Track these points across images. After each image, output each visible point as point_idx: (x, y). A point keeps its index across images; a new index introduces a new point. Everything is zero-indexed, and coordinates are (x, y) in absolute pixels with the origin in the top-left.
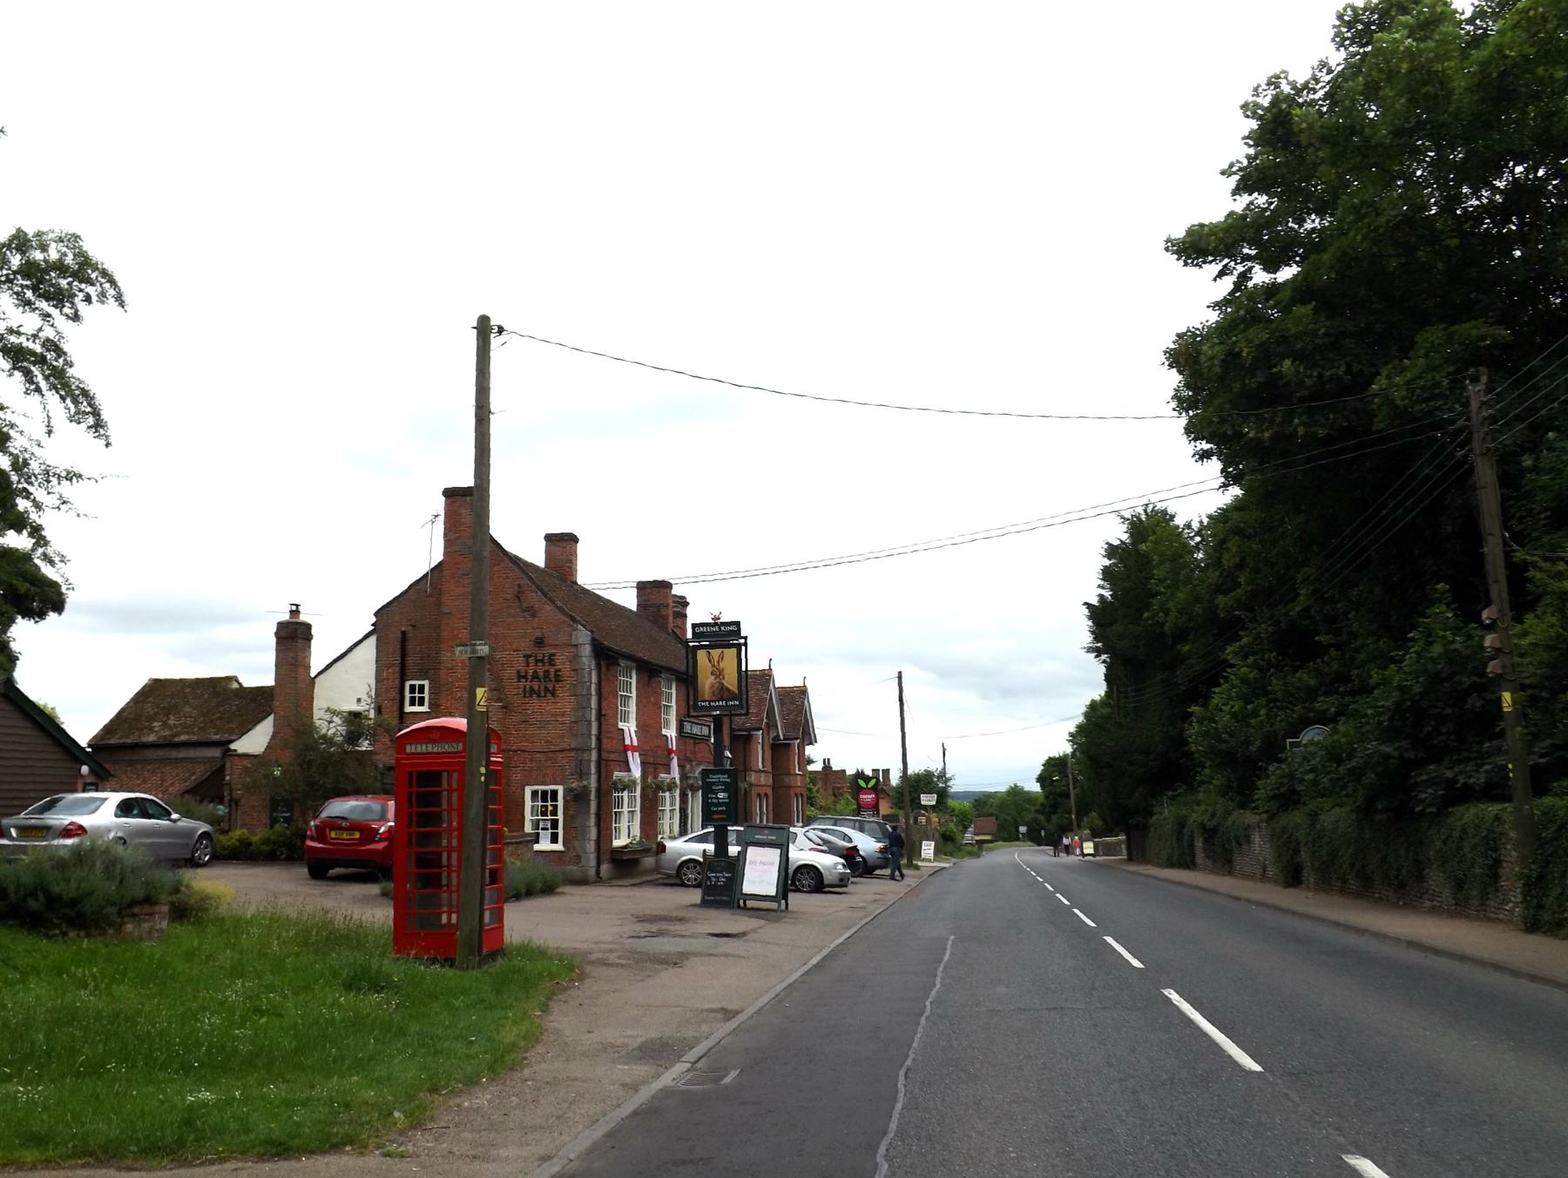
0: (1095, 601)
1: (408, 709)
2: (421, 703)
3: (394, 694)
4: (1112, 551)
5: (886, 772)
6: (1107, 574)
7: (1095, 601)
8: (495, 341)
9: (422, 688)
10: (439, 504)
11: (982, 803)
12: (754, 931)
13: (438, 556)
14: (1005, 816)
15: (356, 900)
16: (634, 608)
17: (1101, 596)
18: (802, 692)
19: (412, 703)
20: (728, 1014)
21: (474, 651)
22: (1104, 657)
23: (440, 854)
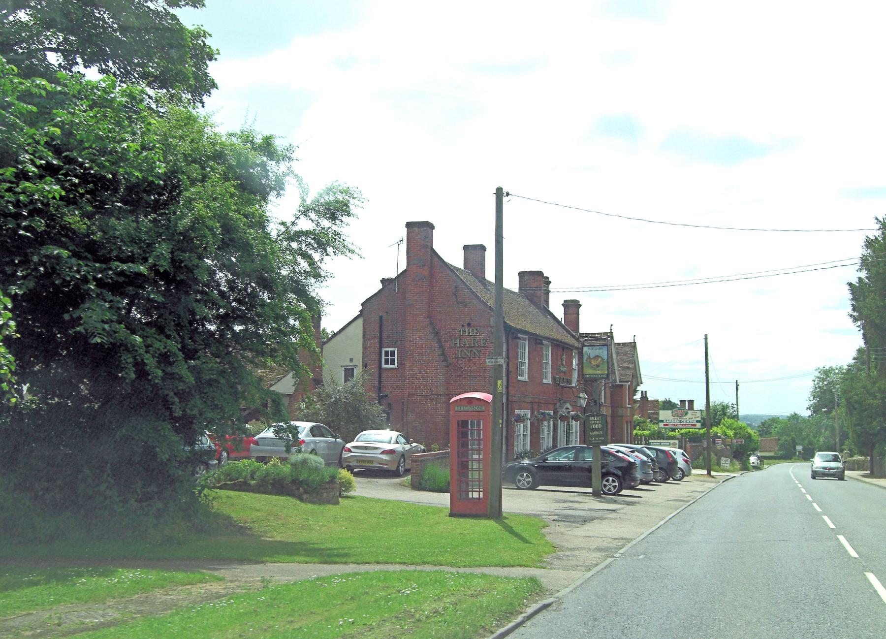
0: (855, 281)
1: (384, 366)
2: (393, 362)
3: (375, 356)
4: (869, 243)
5: (691, 403)
6: (865, 263)
7: (855, 281)
8: (505, 199)
9: (393, 353)
10: (403, 233)
11: (767, 426)
12: (622, 509)
13: (403, 266)
14: (785, 440)
15: (395, 486)
16: (516, 290)
17: (860, 278)
18: (633, 345)
19: (387, 363)
20: (629, 540)
21: (496, 362)
22: (859, 323)
23: (467, 462)
